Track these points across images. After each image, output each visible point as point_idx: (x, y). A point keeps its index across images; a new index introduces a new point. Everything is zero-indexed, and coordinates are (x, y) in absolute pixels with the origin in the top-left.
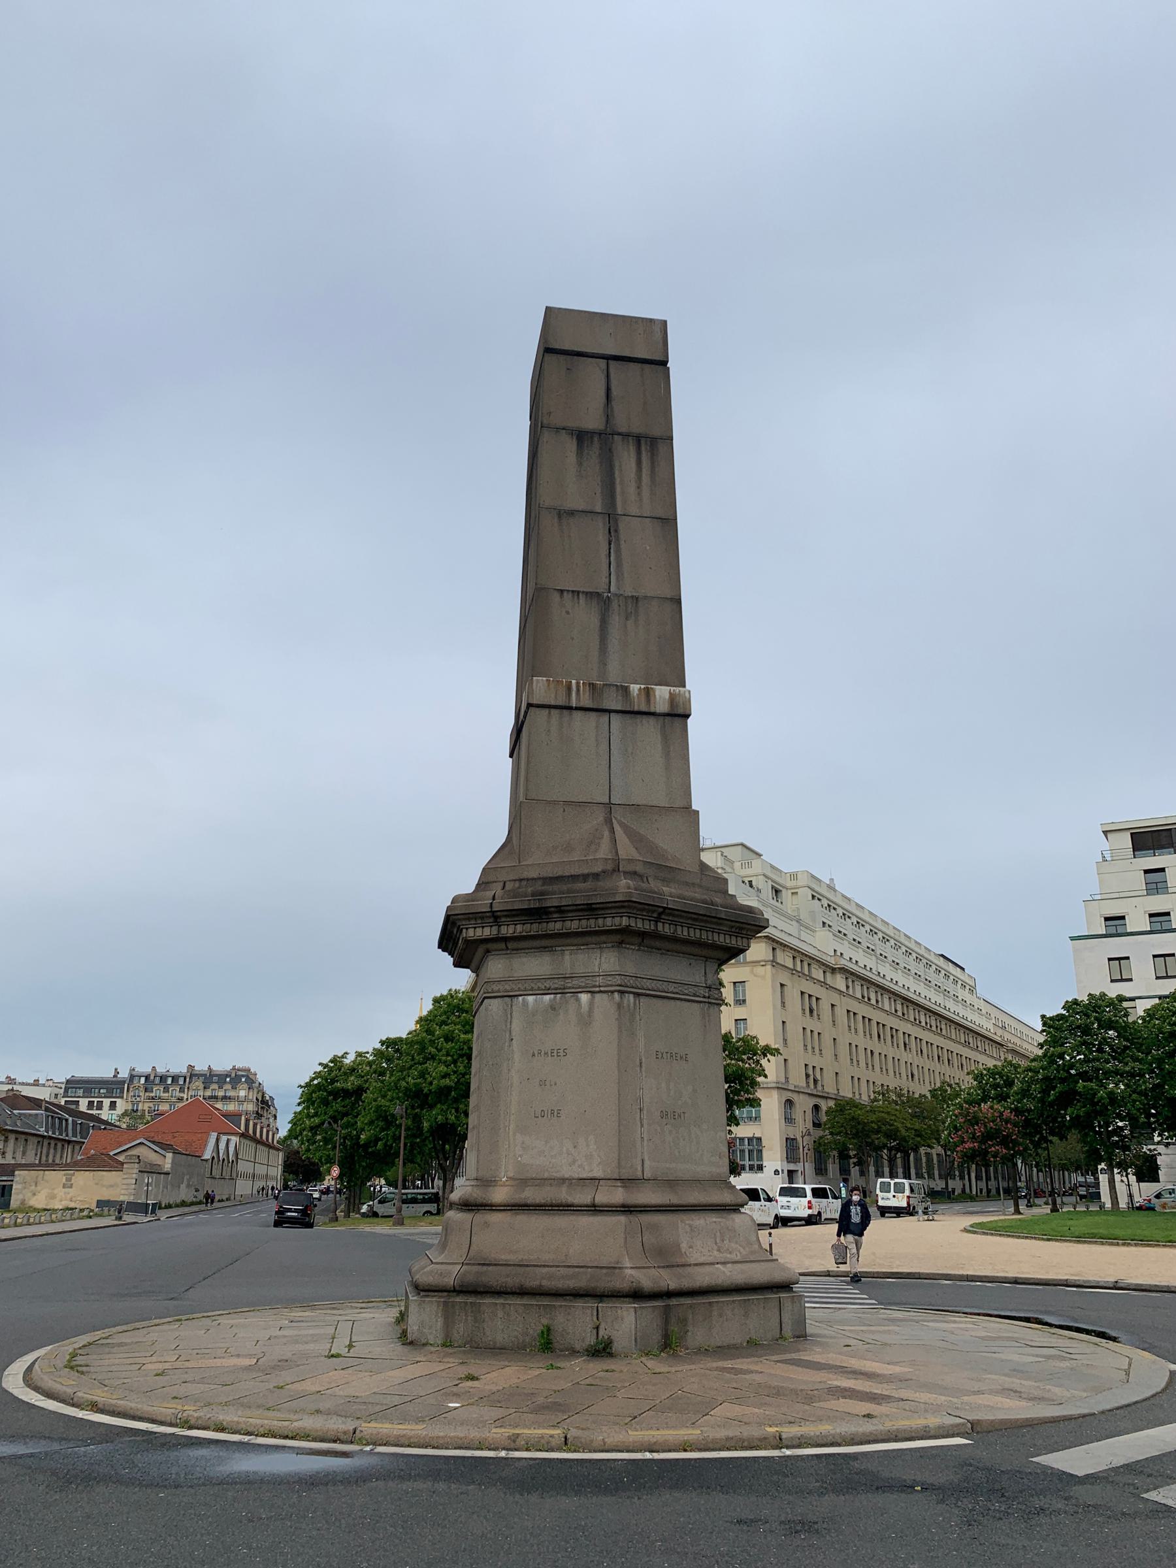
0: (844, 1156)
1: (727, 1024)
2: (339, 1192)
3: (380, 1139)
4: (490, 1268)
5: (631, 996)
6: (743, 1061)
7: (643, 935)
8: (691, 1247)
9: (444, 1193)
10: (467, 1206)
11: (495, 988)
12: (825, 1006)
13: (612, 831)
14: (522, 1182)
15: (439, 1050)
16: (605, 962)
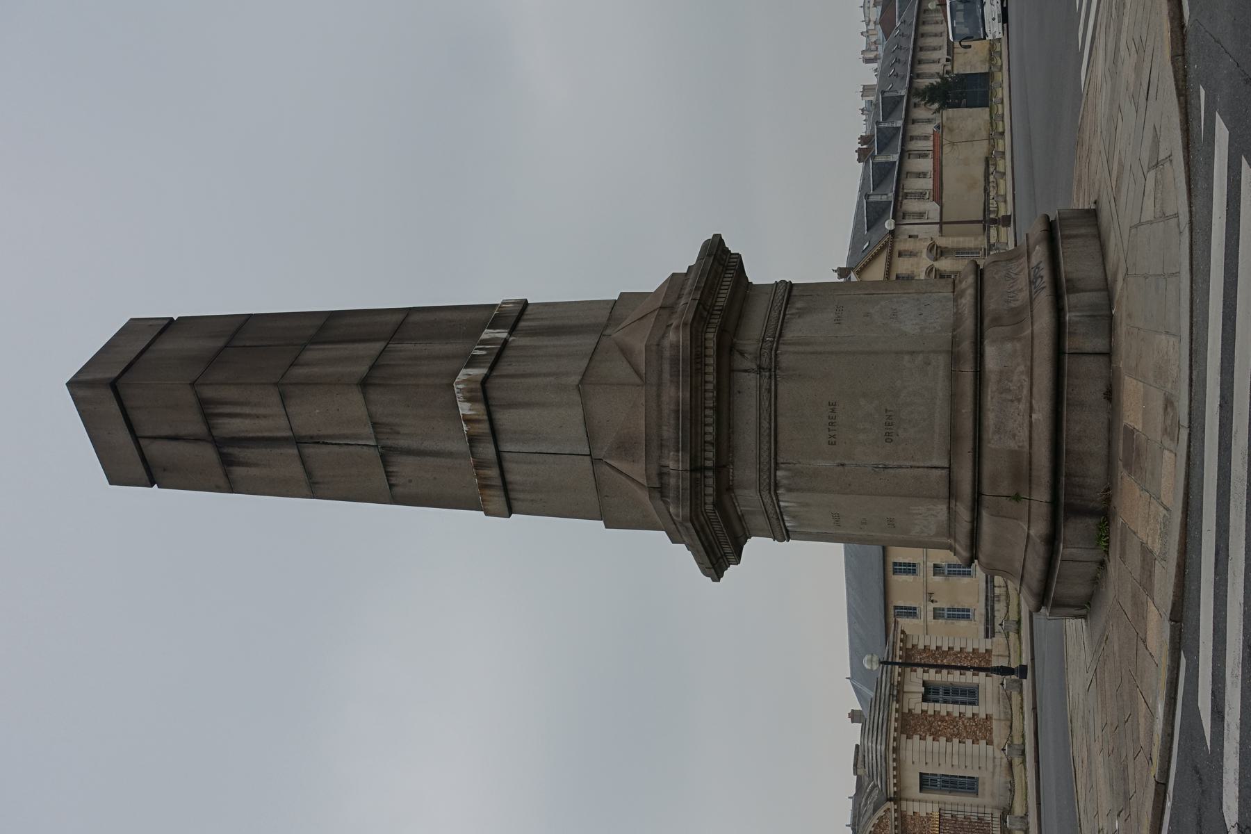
5: (779, 473)
8: (1014, 436)
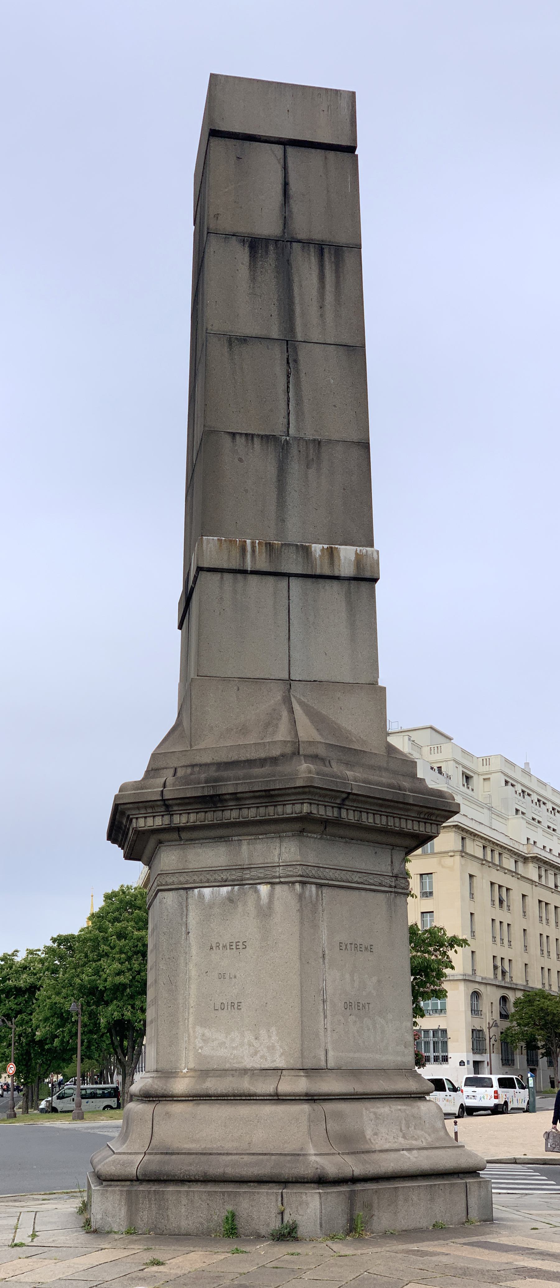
0: (531, 1047)
1: (413, 918)
2: (17, 1089)
3: (57, 1037)
4: (174, 1157)
5: (313, 888)
6: (429, 952)
7: (325, 823)
8: (376, 1134)
9: (123, 1088)
10: (148, 1097)
11: (169, 879)
12: (516, 897)
13: (291, 711)
14: (204, 1073)
15: (112, 948)
16: (285, 852)
